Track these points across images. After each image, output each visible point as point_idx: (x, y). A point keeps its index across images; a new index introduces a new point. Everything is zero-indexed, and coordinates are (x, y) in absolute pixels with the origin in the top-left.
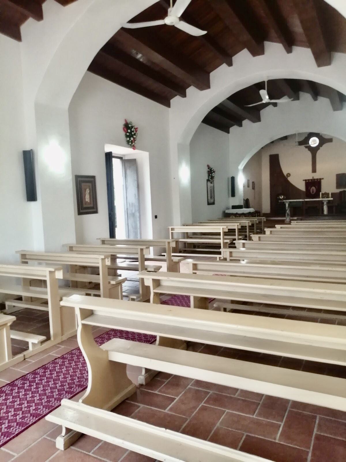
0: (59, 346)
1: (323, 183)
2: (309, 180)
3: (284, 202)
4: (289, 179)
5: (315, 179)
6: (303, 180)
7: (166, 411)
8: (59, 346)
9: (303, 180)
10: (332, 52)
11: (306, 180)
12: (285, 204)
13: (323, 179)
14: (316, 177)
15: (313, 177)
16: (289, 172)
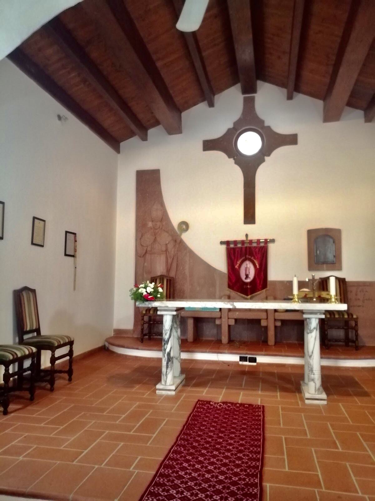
0: (12, 423)
1: (273, 251)
2: (235, 242)
3: (156, 309)
4: (186, 237)
5: (251, 242)
6: (222, 243)
7: (131, 433)
8: (12, 423)
9: (222, 243)
10: (226, 245)
11: (228, 243)
12: (162, 316)
13: (273, 241)
14: (253, 237)
15: (247, 235)
16: (185, 219)
